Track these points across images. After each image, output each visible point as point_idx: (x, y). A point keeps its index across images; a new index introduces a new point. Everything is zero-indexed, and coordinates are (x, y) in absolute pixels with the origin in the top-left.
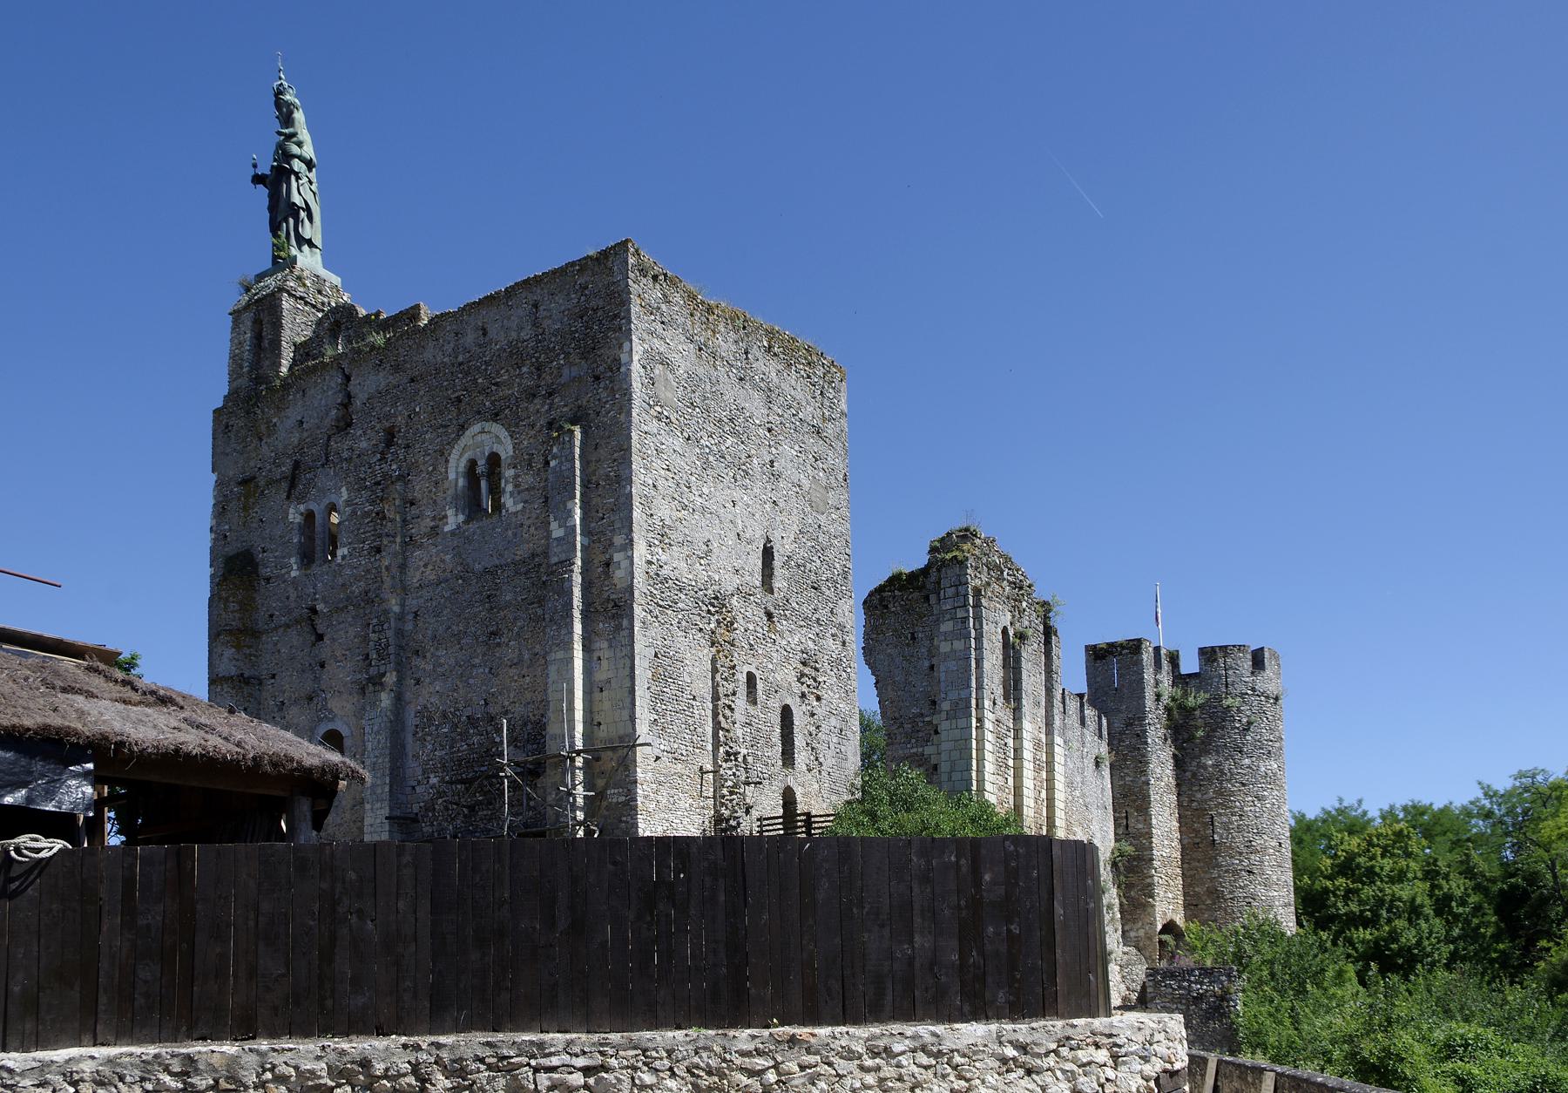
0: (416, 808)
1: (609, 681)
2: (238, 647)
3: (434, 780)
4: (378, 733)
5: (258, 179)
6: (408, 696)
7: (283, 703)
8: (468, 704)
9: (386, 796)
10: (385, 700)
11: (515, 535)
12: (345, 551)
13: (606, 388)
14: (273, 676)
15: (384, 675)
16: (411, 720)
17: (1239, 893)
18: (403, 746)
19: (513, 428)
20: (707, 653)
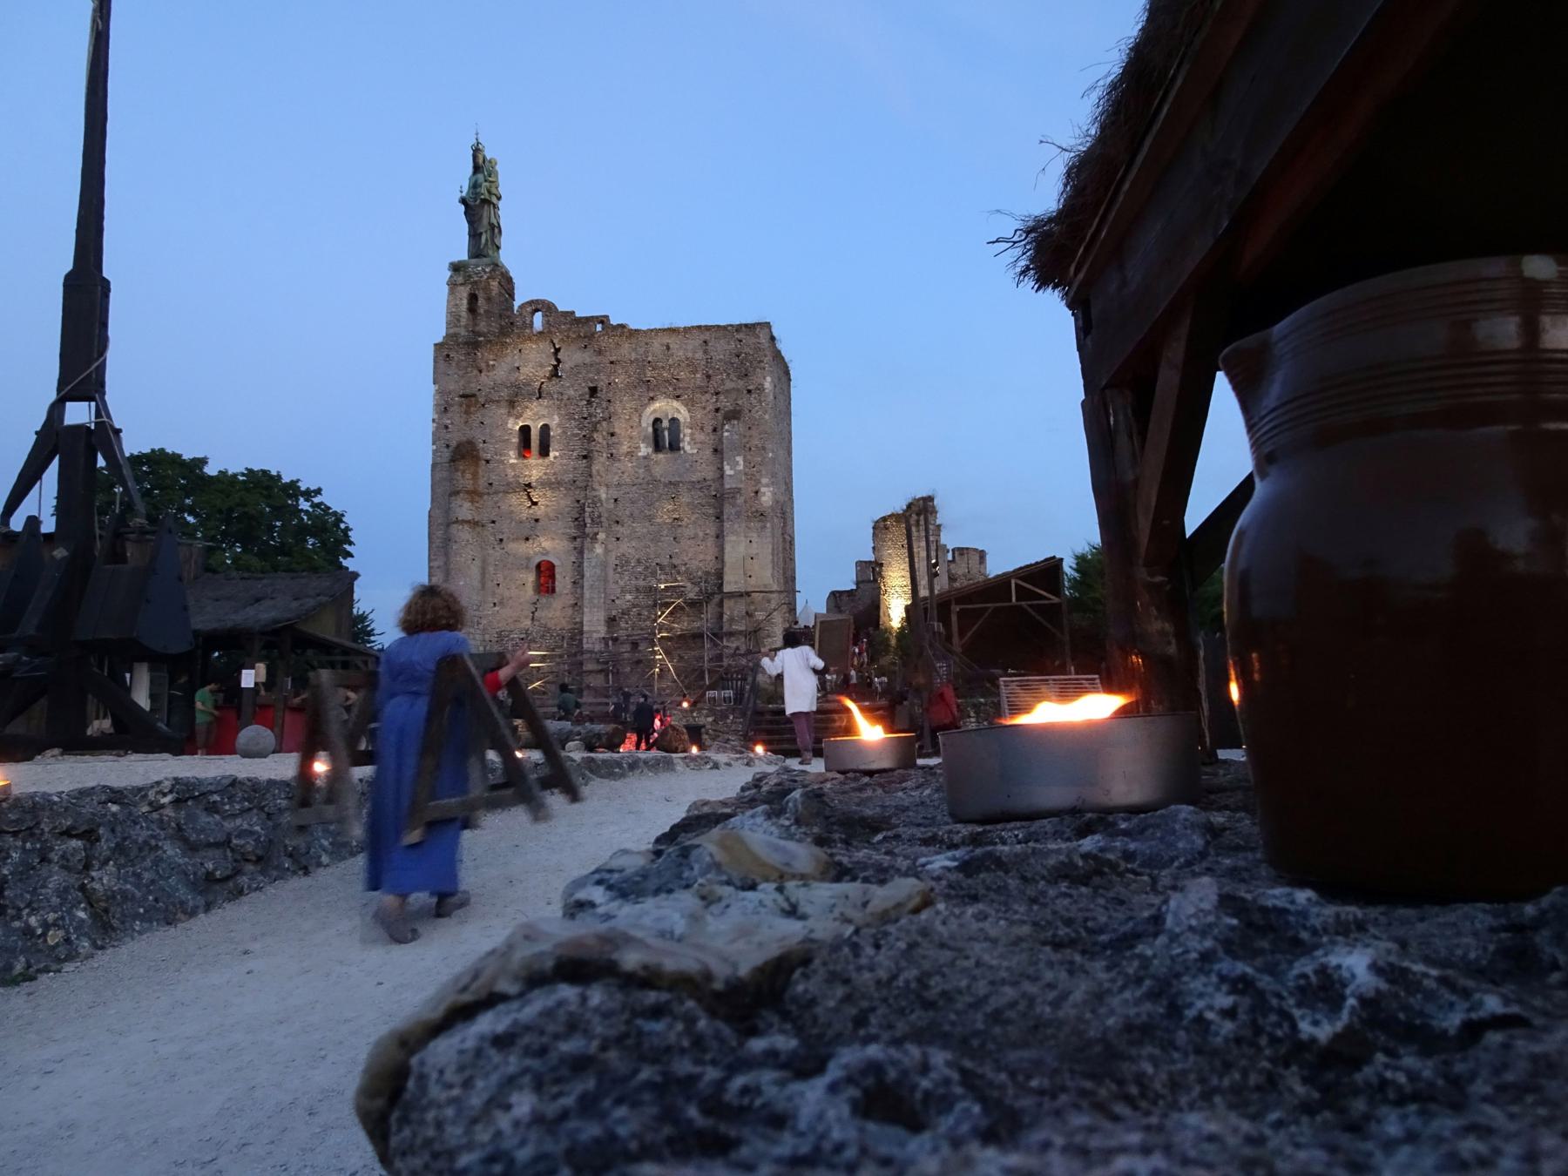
2: (472, 502)
3: (628, 597)
19: (690, 404)
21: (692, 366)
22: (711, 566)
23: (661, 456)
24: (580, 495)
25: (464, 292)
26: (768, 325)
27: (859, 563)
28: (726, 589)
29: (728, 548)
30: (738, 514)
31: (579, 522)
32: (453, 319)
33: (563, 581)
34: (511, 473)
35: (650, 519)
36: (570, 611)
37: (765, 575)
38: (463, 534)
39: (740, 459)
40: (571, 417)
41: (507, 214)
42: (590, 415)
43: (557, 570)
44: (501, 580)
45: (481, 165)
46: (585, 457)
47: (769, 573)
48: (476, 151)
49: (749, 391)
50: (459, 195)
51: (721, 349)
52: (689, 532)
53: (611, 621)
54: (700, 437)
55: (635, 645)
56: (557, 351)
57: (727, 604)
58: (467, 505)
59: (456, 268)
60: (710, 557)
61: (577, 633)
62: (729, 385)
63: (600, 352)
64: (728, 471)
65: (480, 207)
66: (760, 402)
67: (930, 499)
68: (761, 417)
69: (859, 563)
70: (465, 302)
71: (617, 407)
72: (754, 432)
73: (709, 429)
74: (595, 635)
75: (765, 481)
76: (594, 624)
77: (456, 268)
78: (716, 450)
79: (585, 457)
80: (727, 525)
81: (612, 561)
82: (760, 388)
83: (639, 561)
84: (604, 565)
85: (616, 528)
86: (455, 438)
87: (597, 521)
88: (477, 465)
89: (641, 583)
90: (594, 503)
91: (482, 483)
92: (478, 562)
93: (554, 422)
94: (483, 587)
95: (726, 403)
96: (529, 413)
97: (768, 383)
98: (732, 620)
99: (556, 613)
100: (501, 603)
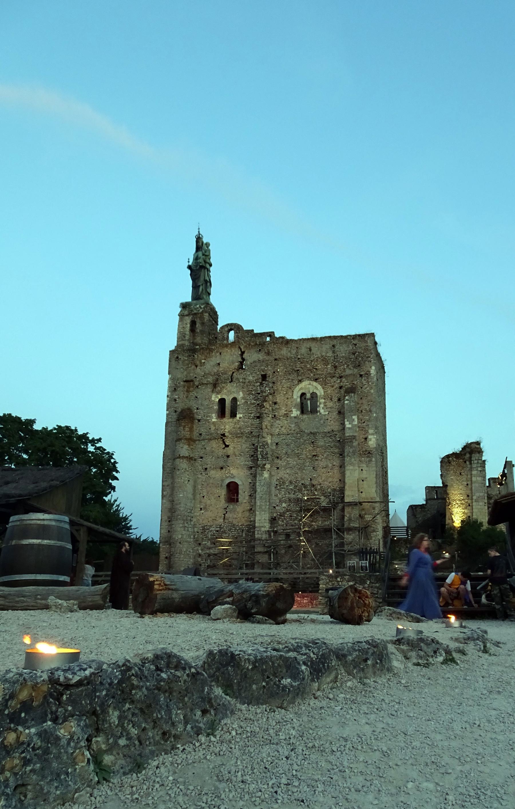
1: (366, 478)
2: (189, 445)
3: (284, 505)
7: (206, 469)
12: (241, 416)
13: (365, 380)
14: (202, 458)
15: (265, 465)
19: (324, 384)
21: (325, 361)
22: (337, 486)
23: (305, 416)
24: (254, 440)
25: (188, 320)
26: (373, 335)
28: (347, 500)
29: (348, 473)
30: (354, 453)
31: (254, 457)
32: (181, 336)
33: (243, 495)
36: (247, 514)
37: (371, 492)
38: (183, 465)
39: (355, 417)
41: (215, 274)
42: (262, 392)
43: (240, 487)
44: (205, 494)
45: (201, 247)
46: (258, 417)
47: (374, 490)
48: (199, 239)
49: (361, 376)
51: (343, 350)
53: (273, 520)
54: (330, 404)
55: (288, 536)
56: (243, 353)
57: (347, 510)
58: (186, 447)
60: (336, 480)
61: (251, 527)
62: (348, 372)
63: (268, 354)
64: (348, 425)
65: (200, 271)
66: (368, 382)
67: (478, 443)
69: (428, 488)
70: (189, 325)
71: (278, 386)
72: (364, 401)
73: (336, 399)
74: (263, 529)
75: (371, 431)
76: (262, 521)
77: (184, 306)
78: (340, 412)
79: (258, 417)
80: (347, 459)
81: (274, 482)
82: (368, 374)
84: (269, 485)
85: (276, 461)
86: (180, 406)
87: (265, 457)
88: (192, 422)
89: (292, 496)
90: (263, 445)
92: (191, 482)
93: (240, 395)
94: (194, 499)
95: (346, 383)
97: (373, 370)
98: (350, 520)
99: (238, 514)
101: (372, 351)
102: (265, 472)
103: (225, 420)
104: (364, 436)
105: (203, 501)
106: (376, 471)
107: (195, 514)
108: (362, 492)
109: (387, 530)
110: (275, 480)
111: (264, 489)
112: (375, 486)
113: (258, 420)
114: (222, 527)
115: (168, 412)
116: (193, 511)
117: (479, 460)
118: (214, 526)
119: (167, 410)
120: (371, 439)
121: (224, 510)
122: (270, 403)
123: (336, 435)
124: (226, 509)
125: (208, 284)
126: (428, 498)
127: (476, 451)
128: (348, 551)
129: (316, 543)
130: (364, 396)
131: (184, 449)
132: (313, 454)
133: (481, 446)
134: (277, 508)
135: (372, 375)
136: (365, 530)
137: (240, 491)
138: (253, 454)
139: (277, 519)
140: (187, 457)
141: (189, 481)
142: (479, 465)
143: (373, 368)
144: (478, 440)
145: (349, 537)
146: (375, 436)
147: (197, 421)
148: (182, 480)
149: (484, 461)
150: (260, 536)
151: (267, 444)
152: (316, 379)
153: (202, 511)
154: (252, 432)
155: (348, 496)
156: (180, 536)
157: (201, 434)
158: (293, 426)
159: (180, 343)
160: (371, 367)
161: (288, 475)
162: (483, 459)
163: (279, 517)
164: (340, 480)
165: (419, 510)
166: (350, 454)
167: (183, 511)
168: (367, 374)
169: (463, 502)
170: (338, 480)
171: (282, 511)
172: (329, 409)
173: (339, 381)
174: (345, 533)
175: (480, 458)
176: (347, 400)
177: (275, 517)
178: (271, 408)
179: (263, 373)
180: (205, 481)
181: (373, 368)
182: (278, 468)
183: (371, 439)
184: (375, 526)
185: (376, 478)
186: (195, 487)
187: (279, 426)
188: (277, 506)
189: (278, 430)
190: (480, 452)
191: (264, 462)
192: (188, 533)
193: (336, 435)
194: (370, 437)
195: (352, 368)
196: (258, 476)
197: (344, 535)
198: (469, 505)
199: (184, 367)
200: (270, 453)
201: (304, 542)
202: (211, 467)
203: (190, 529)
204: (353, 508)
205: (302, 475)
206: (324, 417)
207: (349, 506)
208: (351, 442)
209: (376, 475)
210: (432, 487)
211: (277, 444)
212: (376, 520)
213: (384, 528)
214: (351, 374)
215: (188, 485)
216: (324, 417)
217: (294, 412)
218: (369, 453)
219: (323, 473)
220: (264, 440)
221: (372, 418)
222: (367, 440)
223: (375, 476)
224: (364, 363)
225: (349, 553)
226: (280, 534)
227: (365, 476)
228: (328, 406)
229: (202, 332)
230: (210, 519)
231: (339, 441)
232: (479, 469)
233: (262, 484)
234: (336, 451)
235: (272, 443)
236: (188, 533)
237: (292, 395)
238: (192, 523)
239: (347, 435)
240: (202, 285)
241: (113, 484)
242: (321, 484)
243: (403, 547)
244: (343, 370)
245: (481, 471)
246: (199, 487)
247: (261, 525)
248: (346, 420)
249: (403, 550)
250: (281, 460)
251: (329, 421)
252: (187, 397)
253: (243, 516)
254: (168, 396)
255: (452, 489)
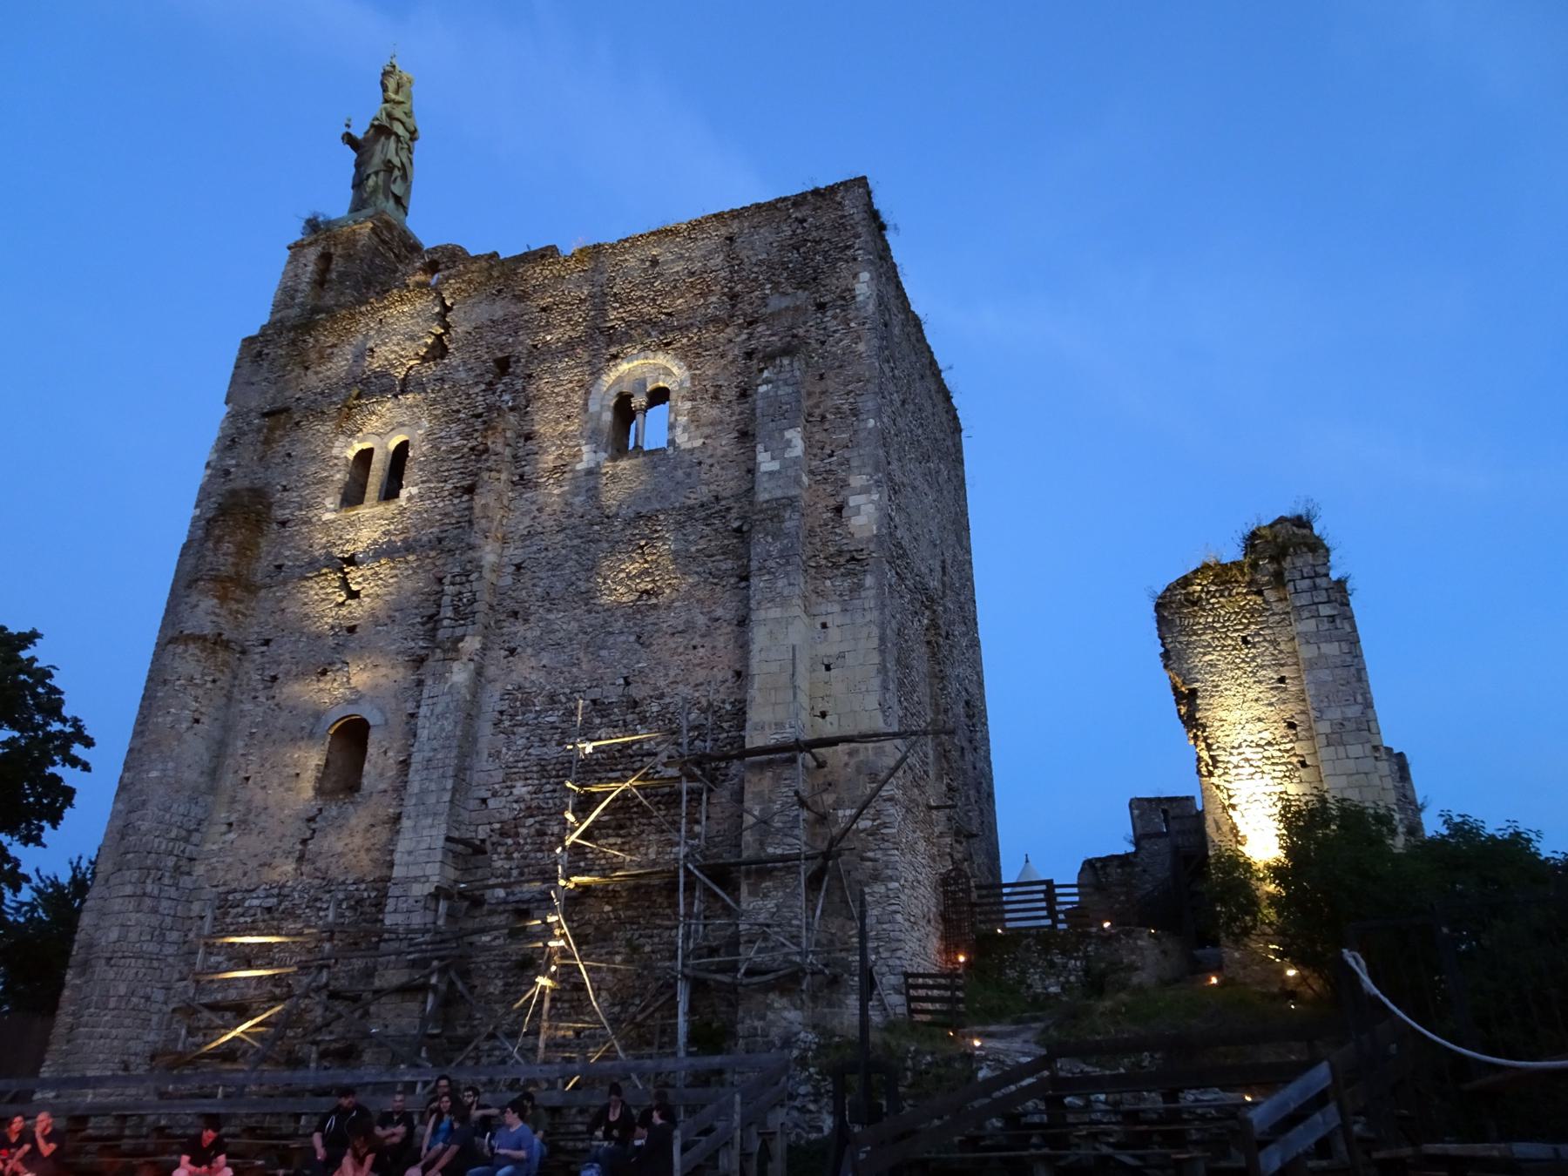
0: (482, 833)
1: (841, 656)
2: (223, 599)
3: (521, 790)
4: (443, 715)
5: (349, 140)
6: (491, 671)
7: (274, 678)
8: (597, 683)
9: (444, 808)
10: (460, 675)
11: (688, 475)
12: (414, 490)
13: (835, 317)
14: (267, 642)
15: (461, 639)
16: (492, 701)
17: (401, 670)
18: (475, 741)
19: (690, 355)
20: (897, 479)
22: (720, 696)
23: (623, 464)
25: (312, 254)
26: (862, 182)
27: (1136, 804)
30: (786, 556)
32: (287, 294)
33: (379, 761)
34: (320, 539)
35: (588, 597)
36: (382, 834)
37: (858, 700)
38: (189, 663)
39: (795, 436)
40: (452, 416)
43: (374, 737)
47: (872, 701)
49: (821, 307)
50: (346, 130)
52: (672, 620)
54: (710, 412)
56: (447, 309)
58: (208, 603)
59: (313, 225)
60: (723, 673)
62: (776, 303)
67: (1302, 522)
68: (848, 351)
69: (1136, 804)
72: (830, 384)
73: (730, 394)
74: (419, 890)
75: (857, 481)
76: (421, 860)
77: (313, 225)
80: (758, 583)
81: (492, 701)
82: (847, 297)
83: (552, 699)
85: (510, 627)
87: (463, 614)
91: (265, 563)
94: (213, 789)
96: (374, 423)
97: (864, 285)
100: (243, 822)
101: (860, 229)
102: (456, 666)
103: (364, 511)
104: (832, 502)
105: (243, 795)
106: (882, 626)
107: (208, 846)
108: (823, 715)
109: (970, 896)
110: (497, 696)
111: (442, 729)
112: (875, 683)
113: (466, 497)
114: (286, 891)
115: (198, 512)
116: (196, 838)
117: (1317, 575)
118: (260, 892)
119: (197, 506)
120: (858, 507)
121: (303, 826)
122: (509, 434)
123: (729, 509)
124: (311, 820)
125: (397, 173)
126: (1139, 831)
127: (1297, 546)
128: (750, 973)
129: (629, 942)
130: (831, 368)
131: (200, 611)
132: (642, 586)
133: (1317, 529)
134: (492, 803)
135: (860, 299)
136: (831, 872)
137: (372, 750)
138: (433, 611)
139: (488, 846)
140: (204, 638)
141: (197, 721)
142: (1323, 597)
143: (865, 276)
144: (1301, 511)
145: (757, 905)
146: (875, 497)
147: (275, 526)
148: (169, 719)
149: (1341, 584)
150: (399, 918)
151: (480, 568)
152: (667, 344)
153: (232, 836)
154: (440, 540)
155: (761, 727)
156: (114, 935)
157: (279, 567)
158: (578, 500)
159: (278, 316)
160: (855, 276)
161: (542, 673)
162: (1334, 576)
163: (495, 838)
164: (738, 674)
165: (1114, 871)
166: (771, 563)
167: (149, 831)
168: (844, 298)
169: (1271, 751)
170: (730, 674)
171: (507, 815)
172: (708, 431)
173: (744, 336)
174: (744, 889)
175: (1321, 570)
176: (767, 381)
177: (483, 841)
178: (508, 451)
179: (500, 355)
180: (264, 723)
181: (865, 276)
182: (512, 652)
183: (858, 507)
184: (879, 855)
185: (882, 652)
186: (220, 749)
187: (534, 507)
188: (494, 795)
189: (527, 521)
190: (1317, 547)
191: (459, 632)
192: (154, 920)
193: (729, 509)
194: (853, 501)
195: (790, 290)
196: (429, 682)
197: (738, 902)
198: (1303, 764)
199: (272, 377)
200: (485, 597)
201: (563, 936)
202: (288, 673)
203: (165, 904)
204: (777, 779)
205: (595, 670)
206: (687, 457)
207: (762, 766)
208: (777, 518)
209: (882, 639)
210: (1149, 800)
211: (518, 567)
212: (884, 825)
213: (951, 886)
214: (787, 308)
215: (189, 736)
216: (687, 457)
217: (585, 457)
218: (853, 559)
219: (674, 652)
220: (471, 554)
221: (863, 435)
222: (844, 513)
223: (875, 642)
224: (833, 266)
225: (756, 979)
226: (491, 913)
227: (835, 650)
228: (703, 420)
229: (343, 276)
230: (253, 864)
231: (739, 530)
232: (1325, 610)
233: (439, 709)
234: (727, 565)
235: (497, 569)
236: (154, 920)
237: (586, 404)
238: (186, 881)
239: (763, 496)
240: (376, 173)
241: (67, 782)
242: (662, 696)
243: (1035, 965)
244: (758, 302)
245: (1332, 618)
246: (240, 744)
247: (415, 871)
248: (760, 447)
249: (1034, 977)
250: (526, 621)
251: (705, 467)
252: (261, 459)
253: (368, 844)
254: (208, 465)
255: (1216, 701)
